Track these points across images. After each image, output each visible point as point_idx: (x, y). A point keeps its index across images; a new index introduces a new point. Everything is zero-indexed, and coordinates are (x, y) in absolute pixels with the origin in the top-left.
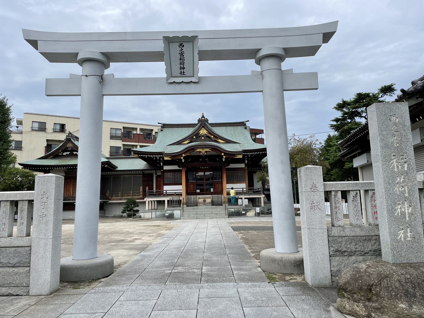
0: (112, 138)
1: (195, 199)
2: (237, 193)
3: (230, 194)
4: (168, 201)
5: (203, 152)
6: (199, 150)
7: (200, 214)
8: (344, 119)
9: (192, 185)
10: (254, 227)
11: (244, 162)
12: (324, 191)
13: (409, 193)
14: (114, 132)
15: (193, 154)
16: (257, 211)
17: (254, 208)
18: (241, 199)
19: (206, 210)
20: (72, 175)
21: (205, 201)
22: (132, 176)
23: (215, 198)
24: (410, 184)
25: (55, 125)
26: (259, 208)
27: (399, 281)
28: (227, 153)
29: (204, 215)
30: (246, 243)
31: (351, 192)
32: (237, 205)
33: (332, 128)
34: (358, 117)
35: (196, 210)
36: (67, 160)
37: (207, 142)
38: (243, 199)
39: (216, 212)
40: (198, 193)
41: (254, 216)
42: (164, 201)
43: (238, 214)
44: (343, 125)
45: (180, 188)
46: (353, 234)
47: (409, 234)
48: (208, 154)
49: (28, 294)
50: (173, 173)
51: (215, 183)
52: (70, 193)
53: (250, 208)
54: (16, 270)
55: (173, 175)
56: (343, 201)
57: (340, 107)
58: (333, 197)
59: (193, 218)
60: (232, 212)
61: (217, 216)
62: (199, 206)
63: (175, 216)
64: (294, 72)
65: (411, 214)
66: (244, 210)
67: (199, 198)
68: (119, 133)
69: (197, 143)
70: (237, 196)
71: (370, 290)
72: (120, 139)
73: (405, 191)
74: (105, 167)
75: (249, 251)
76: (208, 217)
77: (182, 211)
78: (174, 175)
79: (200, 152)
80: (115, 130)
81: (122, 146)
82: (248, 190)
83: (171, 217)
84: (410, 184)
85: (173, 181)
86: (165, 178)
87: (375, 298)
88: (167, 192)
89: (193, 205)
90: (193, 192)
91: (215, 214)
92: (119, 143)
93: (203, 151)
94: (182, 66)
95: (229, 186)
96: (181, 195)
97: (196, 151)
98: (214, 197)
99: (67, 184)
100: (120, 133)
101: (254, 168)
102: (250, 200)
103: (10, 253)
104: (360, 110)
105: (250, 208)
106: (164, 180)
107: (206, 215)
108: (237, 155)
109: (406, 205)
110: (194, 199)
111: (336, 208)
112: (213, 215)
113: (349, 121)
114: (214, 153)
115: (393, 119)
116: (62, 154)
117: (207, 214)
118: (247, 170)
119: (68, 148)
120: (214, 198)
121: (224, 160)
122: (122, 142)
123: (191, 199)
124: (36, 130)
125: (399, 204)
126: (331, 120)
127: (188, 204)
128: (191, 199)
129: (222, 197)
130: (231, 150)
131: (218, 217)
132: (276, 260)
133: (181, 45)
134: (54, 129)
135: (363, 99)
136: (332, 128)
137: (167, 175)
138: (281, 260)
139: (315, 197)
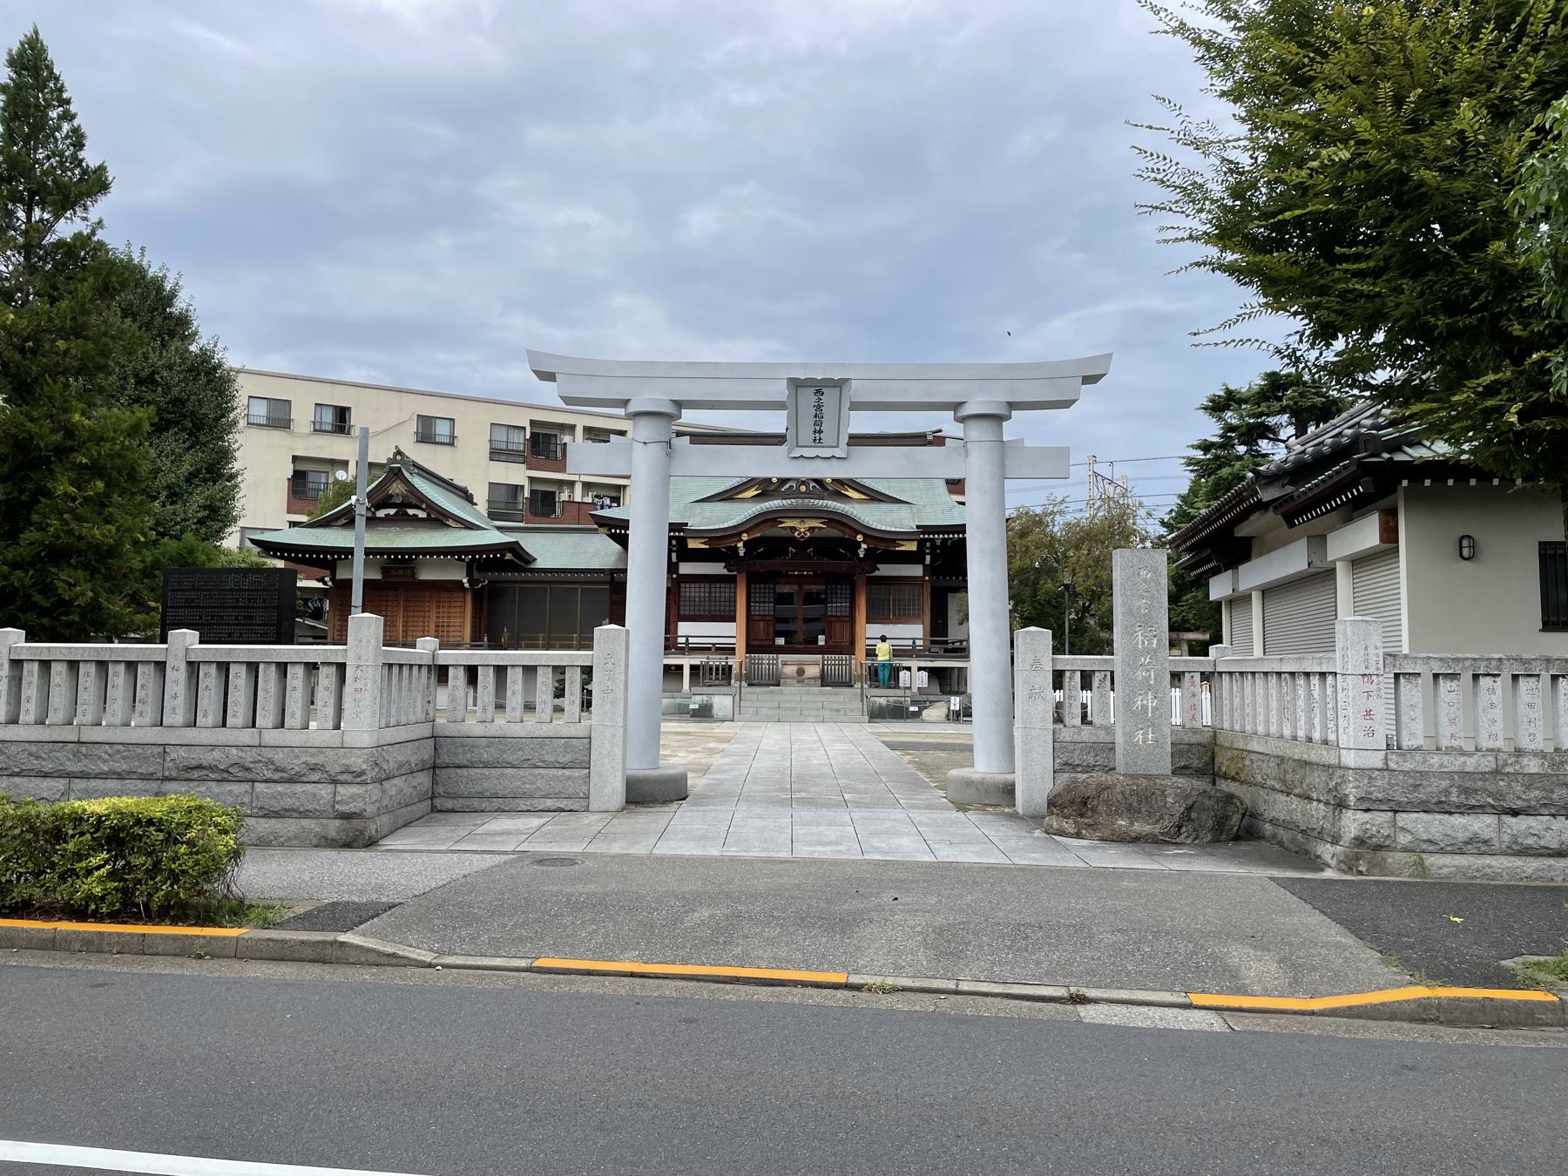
0: (496, 457)
1: (773, 664)
2: (897, 653)
3: (877, 656)
4: (694, 668)
5: (802, 530)
6: (789, 523)
7: (789, 709)
8: (1226, 444)
9: (762, 623)
10: (941, 744)
11: (922, 561)
12: (1054, 671)
13: (1155, 679)
14: (501, 435)
15: (770, 532)
16: (952, 708)
17: (945, 697)
18: (909, 669)
19: (804, 698)
20: (404, 580)
21: (801, 672)
22: (579, 587)
23: (831, 665)
24: (1159, 667)
25: (319, 408)
26: (958, 699)
27: (1123, 793)
28: (872, 536)
29: (798, 712)
30: (921, 770)
31: (1097, 674)
32: (897, 686)
33: (1191, 468)
34: (1265, 441)
35: (778, 698)
36: (390, 534)
37: (816, 501)
38: (914, 669)
39: (835, 706)
40: (780, 646)
41: (945, 719)
42: (680, 668)
43: (897, 713)
44: (1219, 463)
45: (730, 632)
46: (1094, 739)
47: (1150, 736)
48: (816, 533)
49: (587, 810)
50: (707, 585)
51: (831, 619)
52: (398, 632)
53: (932, 698)
54: (568, 772)
55: (707, 590)
56: (1204, 687)
57: (1217, 406)
58: (1067, 680)
59: (769, 719)
60: (881, 707)
61: (838, 716)
62: (785, 685)
63: (715, 710)
64: (1027, 444)
65: (1155, 709)
66: (914, 703)
67: (785, 664)
68: (519, 441)
69: (784, 501)
70: (897, 662)
71: (1085, 804)
72: (521, 460)
73: (1150, 676)
74: (507, 558)
75: (927, 780)
76: (812, 719)
77: (737, 697)
78: (710, 592)
79: (794, 529)
80: (504, 430)
81: (526, 483)
82: (928, 643)
83: (704, 713)
84: (1159, 667)
85: (707, 608)
86: (682, 599)
87: (1089, 813)
88: (691, 640)
89: (764, 682)
90: (766, 643)
91: (832, 710)
92: (517, 474)
93: (803, 527)
94: (818, 428)
95: (874, 630)
96: (730, 650)
97: (783, 525)
98: (828, 660)
99: (387, 606)
100: (522, 441)
101: (951, 578)
102: (935, 673)
103: (559, 746)
104: (1272, 421)
105: (932, 698)
106: (679, 605)
107: (806, 712)
108: (901, 543)
109: (1150, 696)
110: (769, 664)
111: (1070, 697)
112: (827, 714)
113: (1242, 449)
114: (834, 532)
115: (1143, 573)
116: (374, 513)
117: (808, 709)
118: (929, 584)
119: (391, 496)
120: (828, 665)
121: (861, 556)
122: (528, 469)
123: (762, 664)
124: (260, 425)
125: (1141, 694)
126: (1188, 446)
127: (753, 680)
128: (762, 664)
129: (853, 661)
130: (883, 528)
131: (842, 718)
132: (972, 782)
133: (819, 392)
134: (314, 423)
135: (1285, 388)
136: (1191, 468)
137: (687, 590)
138: (982, 783)
139: (1038, 679)
